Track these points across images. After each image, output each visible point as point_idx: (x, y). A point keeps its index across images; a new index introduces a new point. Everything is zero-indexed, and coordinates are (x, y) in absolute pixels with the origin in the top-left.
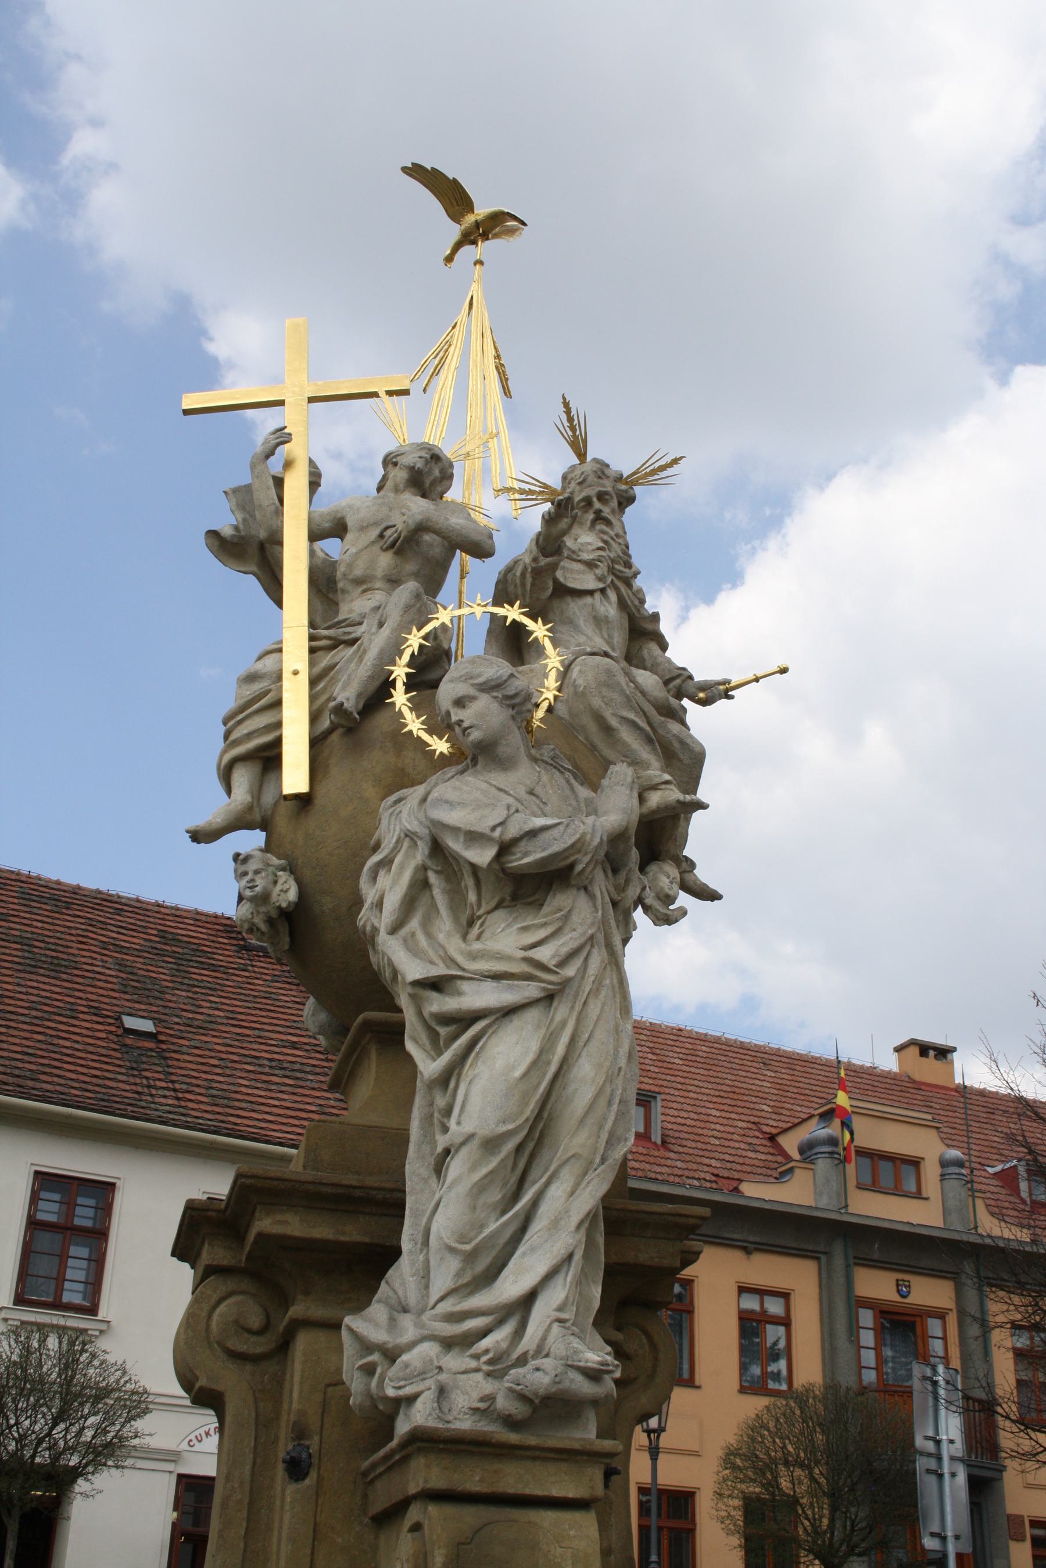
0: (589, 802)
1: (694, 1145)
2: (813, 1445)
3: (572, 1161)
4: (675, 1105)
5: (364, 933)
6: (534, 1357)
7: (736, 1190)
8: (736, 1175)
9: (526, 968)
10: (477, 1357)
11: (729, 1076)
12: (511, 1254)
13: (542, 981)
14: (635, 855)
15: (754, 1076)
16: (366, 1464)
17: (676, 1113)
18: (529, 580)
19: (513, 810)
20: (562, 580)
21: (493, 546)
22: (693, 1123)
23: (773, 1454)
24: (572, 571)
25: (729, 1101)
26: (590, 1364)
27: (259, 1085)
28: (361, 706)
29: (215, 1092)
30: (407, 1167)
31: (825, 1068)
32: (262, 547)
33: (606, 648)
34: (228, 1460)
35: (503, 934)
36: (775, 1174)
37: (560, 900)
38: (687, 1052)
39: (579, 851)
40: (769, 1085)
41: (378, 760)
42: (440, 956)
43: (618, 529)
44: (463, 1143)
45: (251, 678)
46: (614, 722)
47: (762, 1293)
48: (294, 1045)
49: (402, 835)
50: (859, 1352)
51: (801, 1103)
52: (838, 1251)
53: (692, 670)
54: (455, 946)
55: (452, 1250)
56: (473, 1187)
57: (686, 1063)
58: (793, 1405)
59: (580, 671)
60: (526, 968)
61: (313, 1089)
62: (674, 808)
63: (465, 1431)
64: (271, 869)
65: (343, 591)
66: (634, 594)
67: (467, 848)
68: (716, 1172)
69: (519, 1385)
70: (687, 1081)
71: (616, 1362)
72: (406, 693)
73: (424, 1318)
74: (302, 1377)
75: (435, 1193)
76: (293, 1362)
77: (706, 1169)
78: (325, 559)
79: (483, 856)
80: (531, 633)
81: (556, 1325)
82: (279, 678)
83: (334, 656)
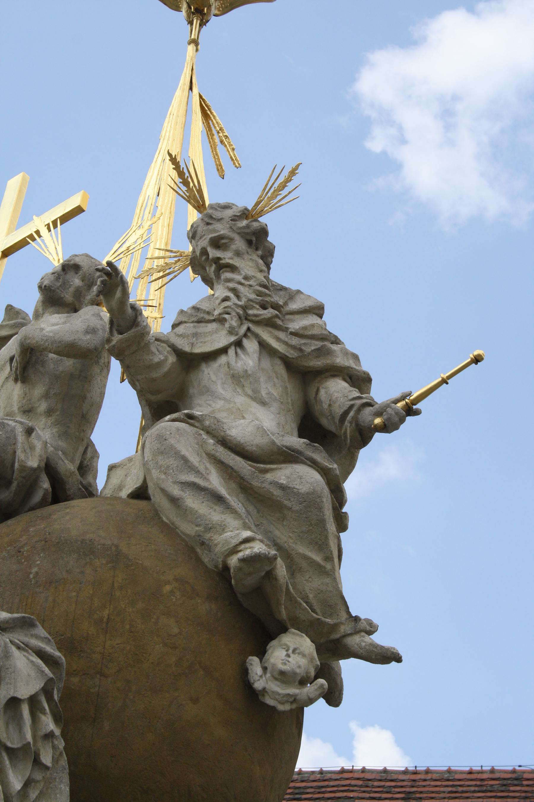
24: (205, 334)
46: (176, 491)
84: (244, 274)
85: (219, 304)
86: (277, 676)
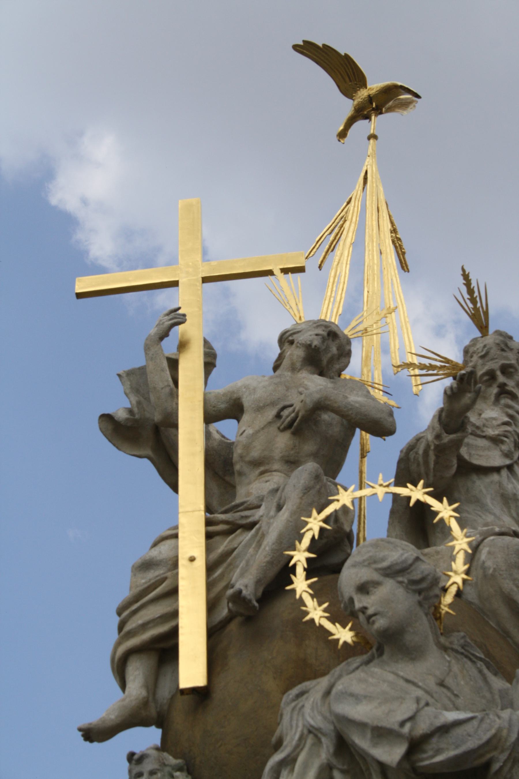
0: (503, 694)
20: (466, 457)
24: (477, 447)
32: (157, 429)
39: (496, 748)
45: (146, 565)
49: (305, 732)
59: (489, 553)
64: (168, 769)
67: (375, 745)
80: (436, 513)
82: (175, 565)
83: (231, 541)
85: (498, 425)
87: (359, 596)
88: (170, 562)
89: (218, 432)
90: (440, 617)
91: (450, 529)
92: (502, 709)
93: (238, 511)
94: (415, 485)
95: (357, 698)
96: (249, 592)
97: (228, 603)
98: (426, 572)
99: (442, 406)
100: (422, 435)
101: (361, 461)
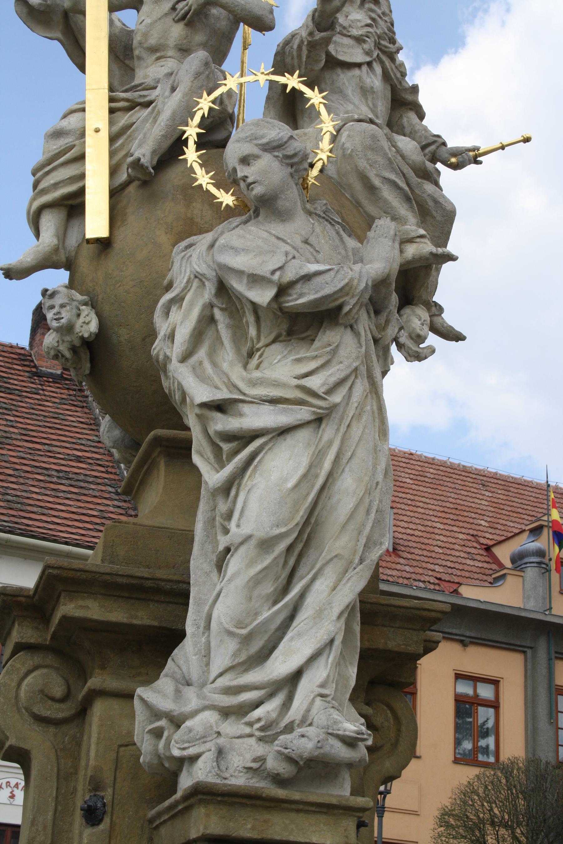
0: (355, 252)
1: (420, 552)
2: (516, 809)
3: (335, 560)
4: (405, 518)
5: (157, 361)
6: (299, 726)
7: (456, 592)
8: (456, 580)
9: (299, 394)
10: (250, 724)
11: (453, 495)
12: (281, 639)
13: (312, 405)
14: (394, 299)
15: (474, 495)
16: (152, 813)
17: (406, 525)
18: (305, 52)
19: (290, 257)
20: (333, 53)
21: (273, 21)
22: (420, 534)
23: (481, 815)
25: (452, 516)
26: (347, 733)
27: (48, 492)
28: (155, 162)
29: (9, 498)
30: (192, 562)
31: (535, 490)
32: (66, 14)
33: (371, 116)
34: (34, 807)
35: (280, 364)
36: (490, 579)
37: (329, 336)
38: (417, 473)
39: (347, 294)
40: (487, 503)
41: (169, 210)
42: (224, 382)
43: (385, 8)
44: (242, 543)
45: (57, 134)
46: (377, 182)
47: (475, 679)
48: (79, 459)
49: (192, 277)
50: (557, 732)
51: (514, 519)
52: (542, 646)
53: (445, 137)
54: (237, 374)
55: (230, 634)
56: (249, 581)
57: (416, 482)
58: (500, 775)
59: (349, 136)
60: (299, 394)
61: (95, 497)
62: (427, 259)
63: (240, 787)
64: (75, 303)
65: (139, 58)
66: (396, 67)
67: (250, 288)
68: (439, 576)
69: (286, 748)
70: (417, 498)
71: (369, 732)
72: (197, 151)
73: (205, 690)
74: (98, 738)
75: (215, 585)
76: (90, 726)
77: (430, 573)
78: (122, 29)
79: (263, 296)
80: (309, 100)
81: (318, 700)
82: (83, 134)
83: (131, 116)
84: (383, 10)
85: (362, 27)
86: (414, 337)
87: (241, 166)
88: (78, 132)
89: (119, 20)
90: (307, 187)
91: (319, 113)
92: (354, 264)
93: (137, 91)
94: (292, 75)
95: (236, 250)
96: (146, 160)
97: (128, 169)
98: (298, 149)
99: (316, 7)
100: (297, 32)
101: (243, 53)
